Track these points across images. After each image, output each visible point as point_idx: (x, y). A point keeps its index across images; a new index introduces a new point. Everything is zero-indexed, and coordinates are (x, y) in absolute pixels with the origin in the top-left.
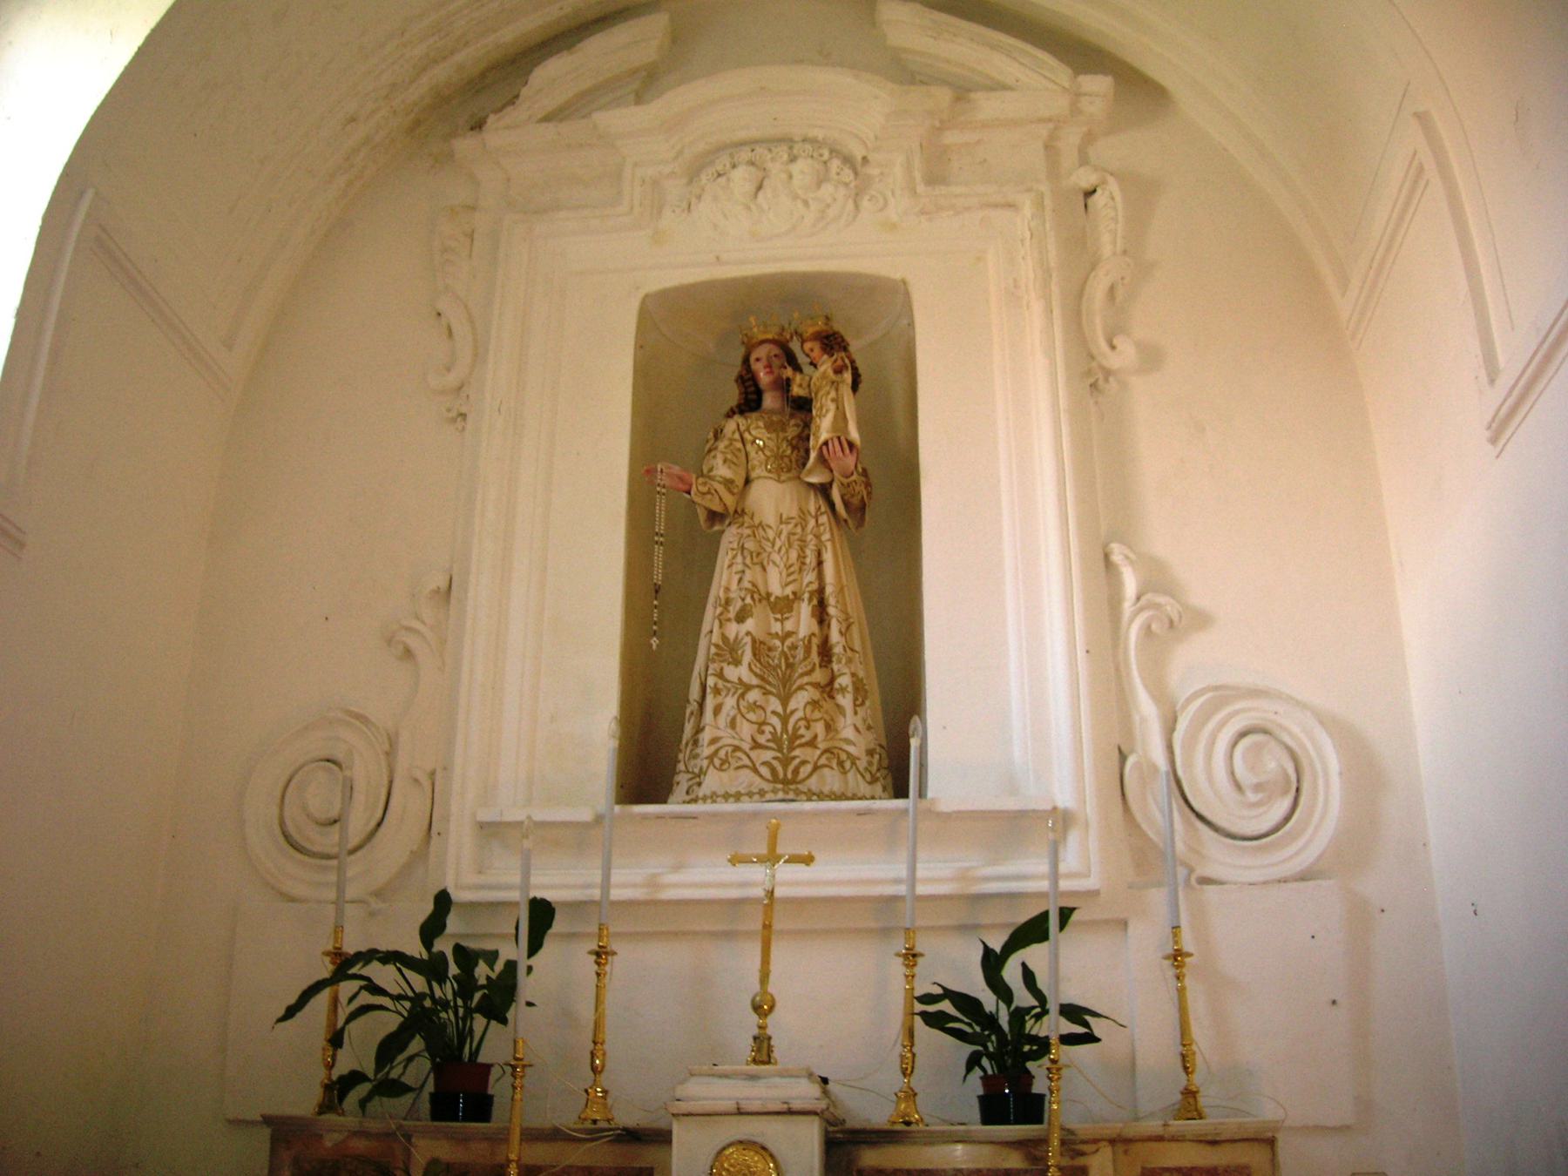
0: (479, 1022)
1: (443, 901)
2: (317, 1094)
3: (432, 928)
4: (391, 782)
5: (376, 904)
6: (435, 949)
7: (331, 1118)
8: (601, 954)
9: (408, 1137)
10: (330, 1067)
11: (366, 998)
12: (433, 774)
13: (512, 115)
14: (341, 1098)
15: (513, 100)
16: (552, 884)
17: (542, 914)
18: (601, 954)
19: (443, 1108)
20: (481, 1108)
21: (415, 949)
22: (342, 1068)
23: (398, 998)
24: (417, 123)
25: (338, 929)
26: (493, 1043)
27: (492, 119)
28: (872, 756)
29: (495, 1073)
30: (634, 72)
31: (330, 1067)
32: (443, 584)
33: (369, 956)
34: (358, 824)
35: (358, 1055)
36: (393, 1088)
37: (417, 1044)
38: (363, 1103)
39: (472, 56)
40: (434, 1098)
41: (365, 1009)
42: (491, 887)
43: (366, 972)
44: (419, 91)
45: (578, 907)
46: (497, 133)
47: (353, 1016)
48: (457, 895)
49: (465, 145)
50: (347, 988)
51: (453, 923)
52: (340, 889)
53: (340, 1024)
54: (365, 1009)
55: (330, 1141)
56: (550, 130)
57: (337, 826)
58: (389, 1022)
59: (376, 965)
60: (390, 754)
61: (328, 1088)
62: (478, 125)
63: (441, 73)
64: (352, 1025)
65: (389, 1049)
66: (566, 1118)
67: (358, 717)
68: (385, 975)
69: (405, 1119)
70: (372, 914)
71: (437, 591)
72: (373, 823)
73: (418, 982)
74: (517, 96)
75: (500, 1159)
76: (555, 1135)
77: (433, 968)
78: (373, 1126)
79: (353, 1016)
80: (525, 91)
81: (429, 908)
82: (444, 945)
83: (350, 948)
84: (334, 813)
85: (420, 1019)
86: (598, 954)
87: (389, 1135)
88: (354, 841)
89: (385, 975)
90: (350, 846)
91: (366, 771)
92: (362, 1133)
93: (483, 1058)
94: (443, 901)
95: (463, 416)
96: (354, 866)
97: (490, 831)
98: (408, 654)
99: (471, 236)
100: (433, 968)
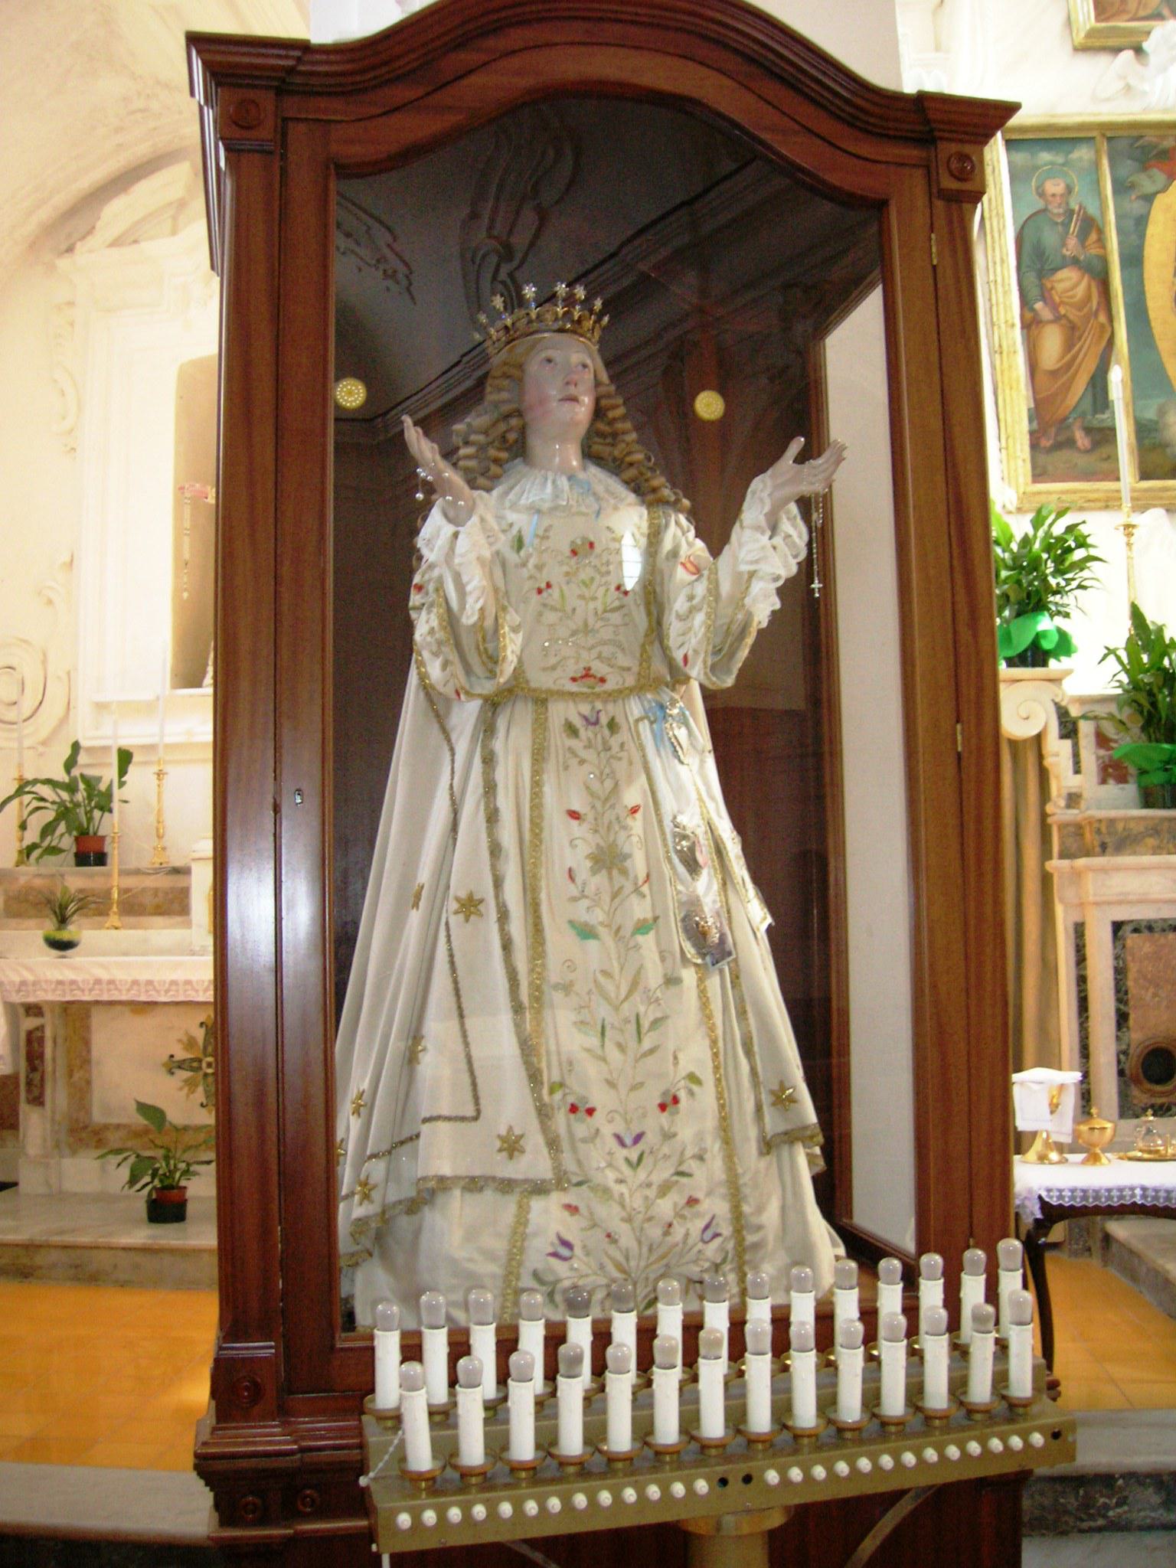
0: (97, 813)
1: (76, 747)
2: (15, 856)
3: (70, 764)
4: (46, 678)
5: (41, 749)
6: (72, 774)
7: (23, 868)
8: (160, 774)
9: (62, 876)
10: (21, 840)
11: (35, 804)
12: (69, 674)
13: (93, 241)
14: (28, 856)
15: (91, 231)
16: (131, 735)
17: (125, 758)
18: (160, 774)
19: (82, 859)
20: (101, 859)
21: (61, 776)
22: (27, 842)
23: (53, 803)
24: (34, 243)
25: (20, 766)
26: (107, 825)
27: (79, 245)
28: (1132, 187)
29: (108, 841)
30: (170, 204)
31: (21, 840)
32: (68, 559)
33: (35, 782)
34: (28, 705)
35: (32, 836)
36: (53, 850)
37: (62, 827)
38: (38, 859)
39: (62, 199)
40: (77, 855)
41: (38, 809)
42: (101, 738)
43: (34, 789)
44: (32, 226)
45: (151, 748)
46: (84, 254)
47: (31, 813)
48: (83, 743)
49: (64, 263)
50: (27, 798)
51: (82, 759)
52: (20, 740)
53: (25, 817)
54: (38, 809)
55: (22, 880)
56: (115, 252)
57: (16, 706)
58: (49, 815)
59: (39, 785)
60: (44, 662)
61: (20, 852)
62: (70, 250)
63: (44, 214)
64: (31, 817)
65: (48, 830)
66: (144, 864)
67: (25, 641)
68: (45, 791)
69: (61, 866)
70: (41, 755)
71: (65, 563)
72: (37, 703)
73: (65, 796)
74: (94, 228)
75: (109, 885)
76: (138, 872)
77: (71, 788)
78: (43, 871)
79: (31, 813)
80: (99, 224)
81: (68, 752)
82: (76, 772)
83: (29, 776)
84: (14, 698)
85: (65, 813)
86: (158, 775)
87: (53, 876)
88: (27, 714)
89: (45, 791)
90: (24, 717)
91: (30, 671)
92: (39, 875)
93: (100, 833)
94: (76, 747)
95: (73, 449)
96: (29, 728)
97: (101, 707)
98: (50, 602)
99: (72, 324)
100: (71, 788)
